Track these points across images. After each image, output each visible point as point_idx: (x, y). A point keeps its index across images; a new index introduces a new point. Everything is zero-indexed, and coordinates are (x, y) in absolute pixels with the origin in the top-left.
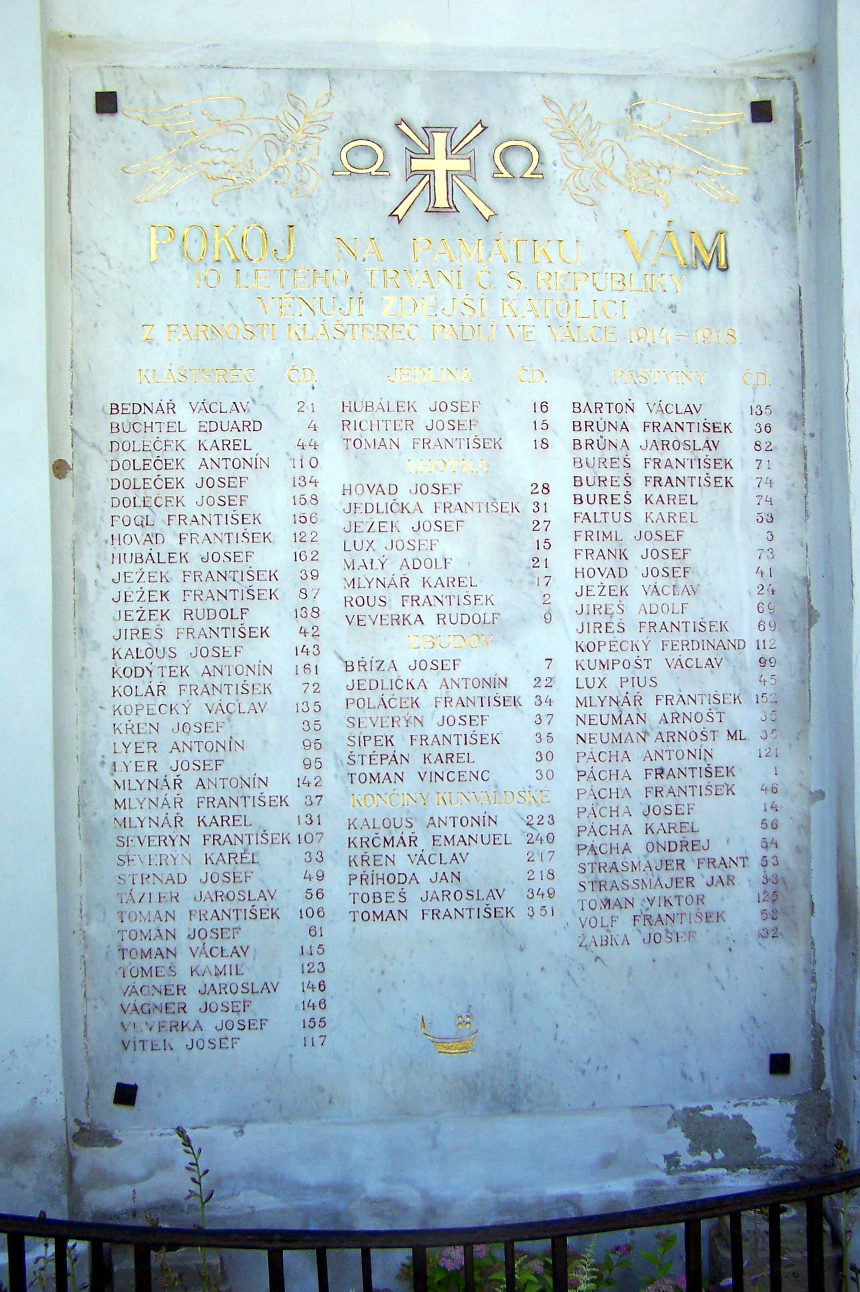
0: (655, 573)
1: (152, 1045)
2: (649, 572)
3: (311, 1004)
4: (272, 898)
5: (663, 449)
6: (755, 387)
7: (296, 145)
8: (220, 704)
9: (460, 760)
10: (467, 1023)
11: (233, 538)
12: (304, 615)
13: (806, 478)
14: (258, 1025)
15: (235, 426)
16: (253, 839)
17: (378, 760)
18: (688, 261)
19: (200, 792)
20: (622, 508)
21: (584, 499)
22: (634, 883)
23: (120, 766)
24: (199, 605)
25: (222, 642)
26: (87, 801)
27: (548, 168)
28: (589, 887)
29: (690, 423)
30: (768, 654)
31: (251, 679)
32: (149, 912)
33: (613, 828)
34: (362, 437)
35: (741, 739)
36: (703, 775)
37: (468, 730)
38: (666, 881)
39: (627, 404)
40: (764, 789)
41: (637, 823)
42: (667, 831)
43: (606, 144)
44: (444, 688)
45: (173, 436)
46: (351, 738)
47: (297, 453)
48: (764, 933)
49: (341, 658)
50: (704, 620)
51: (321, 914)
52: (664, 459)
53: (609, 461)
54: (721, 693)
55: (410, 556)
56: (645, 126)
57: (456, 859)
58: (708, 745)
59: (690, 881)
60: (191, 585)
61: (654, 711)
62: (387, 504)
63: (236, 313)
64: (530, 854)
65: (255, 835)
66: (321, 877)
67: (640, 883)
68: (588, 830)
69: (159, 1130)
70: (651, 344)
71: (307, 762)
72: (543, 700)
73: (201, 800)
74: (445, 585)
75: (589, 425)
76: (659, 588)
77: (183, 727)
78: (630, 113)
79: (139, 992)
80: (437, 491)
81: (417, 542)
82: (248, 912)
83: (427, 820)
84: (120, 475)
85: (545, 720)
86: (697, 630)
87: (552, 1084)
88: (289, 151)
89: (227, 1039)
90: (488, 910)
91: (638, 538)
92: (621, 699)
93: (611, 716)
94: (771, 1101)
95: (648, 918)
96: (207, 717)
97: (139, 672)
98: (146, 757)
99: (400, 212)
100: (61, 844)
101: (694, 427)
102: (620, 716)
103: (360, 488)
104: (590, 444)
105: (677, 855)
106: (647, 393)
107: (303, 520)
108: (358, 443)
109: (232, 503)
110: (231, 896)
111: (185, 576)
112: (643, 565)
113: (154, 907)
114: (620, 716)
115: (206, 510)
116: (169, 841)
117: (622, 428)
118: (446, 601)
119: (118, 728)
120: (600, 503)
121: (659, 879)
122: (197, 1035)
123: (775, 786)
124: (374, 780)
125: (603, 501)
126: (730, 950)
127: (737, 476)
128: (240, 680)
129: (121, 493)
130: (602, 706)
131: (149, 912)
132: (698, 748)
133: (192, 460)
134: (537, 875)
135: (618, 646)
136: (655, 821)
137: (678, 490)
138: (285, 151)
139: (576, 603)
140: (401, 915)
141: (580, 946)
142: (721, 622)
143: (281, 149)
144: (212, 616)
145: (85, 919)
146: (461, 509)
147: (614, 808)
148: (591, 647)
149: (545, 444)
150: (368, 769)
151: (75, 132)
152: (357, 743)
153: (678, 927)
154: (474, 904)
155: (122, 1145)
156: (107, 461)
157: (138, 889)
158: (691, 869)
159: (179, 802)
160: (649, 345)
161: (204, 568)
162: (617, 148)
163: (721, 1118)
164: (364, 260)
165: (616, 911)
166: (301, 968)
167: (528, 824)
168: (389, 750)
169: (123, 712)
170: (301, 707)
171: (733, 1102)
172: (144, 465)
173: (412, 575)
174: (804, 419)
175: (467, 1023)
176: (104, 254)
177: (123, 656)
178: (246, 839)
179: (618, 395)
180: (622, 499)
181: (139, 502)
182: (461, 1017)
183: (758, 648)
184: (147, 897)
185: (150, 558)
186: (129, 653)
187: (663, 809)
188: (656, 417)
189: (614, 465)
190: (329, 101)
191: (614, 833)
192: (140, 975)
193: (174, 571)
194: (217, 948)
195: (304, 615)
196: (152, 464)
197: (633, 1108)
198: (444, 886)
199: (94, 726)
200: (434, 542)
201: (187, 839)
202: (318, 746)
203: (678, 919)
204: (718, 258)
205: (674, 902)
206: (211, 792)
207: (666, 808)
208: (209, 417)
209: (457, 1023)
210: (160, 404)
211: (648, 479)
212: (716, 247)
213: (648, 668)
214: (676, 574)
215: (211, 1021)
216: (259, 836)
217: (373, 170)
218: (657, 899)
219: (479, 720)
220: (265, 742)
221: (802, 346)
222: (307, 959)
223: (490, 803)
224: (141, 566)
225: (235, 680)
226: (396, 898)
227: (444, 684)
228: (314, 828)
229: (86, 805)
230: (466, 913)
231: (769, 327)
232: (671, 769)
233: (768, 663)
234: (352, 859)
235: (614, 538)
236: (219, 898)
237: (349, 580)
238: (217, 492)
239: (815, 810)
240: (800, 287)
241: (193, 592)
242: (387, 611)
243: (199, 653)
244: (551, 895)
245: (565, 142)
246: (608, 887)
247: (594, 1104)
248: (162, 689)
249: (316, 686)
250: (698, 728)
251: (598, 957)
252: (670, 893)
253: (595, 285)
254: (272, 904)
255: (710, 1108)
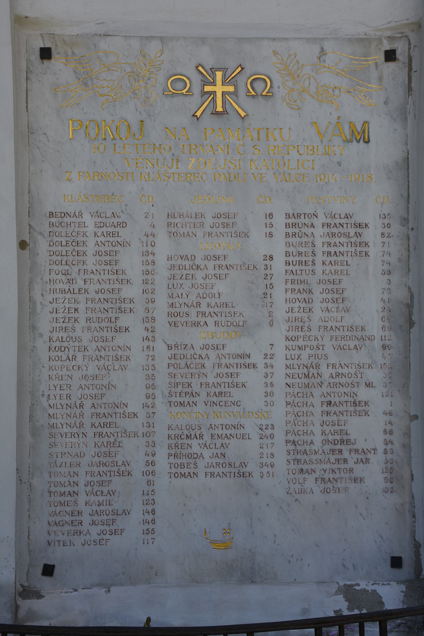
0: (327, 301)
1: (64, 543)
2: (324, 301)
3: (147, 521)
4: (128, 465)
5: (332, 237)
6: (382, 204)
7: (145, 78)
8: (104, 366)
9: (226, 395)
10: (228, 533)
11: (112, 282)
12: (147, 321)
13: (409, 251)
14: (119, 532)
15: (113, 225)
16: (119, 434)
17: (184, 395)
18: (348, 138)
19: (93, 410)
20: (310, 268)
21: (291, 263)
22: (316, 461)
23: (52, 397)
24: (94, 315)
25: (105, 334)
26: (34, 415)
27: (275, 90)
28: (292, 462)
29: (347, 223)
30: (388, 343)
31: (120, 353)
32: (65, 472)
33: (306, 434)
34: (177, 231)
35: (372, 387)
36: (352, 405)
37: (230, 380)
38: (332, 459)
39: (314, 214)
40: (385, 413)
41: (317, 430)
42: (333, 434)
43: (306, 76)
44: (218, 359)
45: (82, 230)
46: (170, 383)
47: (144, 239)
48: (386, 490)
49: (165, 343)
50: (353, 325)
51: (154, 474)
52: (333, 242)
53: (304, 243)
54: (361, 363)
55: (201, 292)
56: (327, 66)
57: (223, 446)
58: (355, 390)
59: (345, 461)
60: (90, 305)
61: (326, 372)
62: (190, 265)
63: (114, 166)
64: (262, 444)
65: (120, 433)
66: (154, 455)
67: (319, 461)
68: (291, 433)
69: (66, 590)
70: (327, 182)
71: (148, 395)
72: (268, 365)
73: (93, 414)
74: (219, 306)
75: (294, 225)
76: (329, 309)
77: (85, 377)
78: (319, 59)
79: (58, 514)
80: (215, 259)
81: (205, 284)
82: (116, 472)
83: (208, 426)
84: (54, 248)
85: (270, 376)
86: (349, 330)
87: (273, 567)
88: (141, 81)
89: (103, 540)
90: (239, 473)
91: (318, 283)
92: (309, 365)
93: (303, 374)
94: (392, 583)
95: (323, 479)
96: (97, 372)
97: (63, 349)
98: (65, 392)
99: (198, 114)
100: (20, 437)
101: (349, 226)
102: (308, 374)
103: (176, 257)
104: (294, 235)
105: (338, 447)
106: (325, 208)
107: (147, 273)
108: (175, 234)
109: (111, 264)
110: (107, 464)
111: (87, 300)
112: (321, 297)
113: (67, 470)
114: (308, 374)
115: (98, 267)
116: (76, 435)
117: (311, 226)
118: (219, 315)
119: (51, 377)
120: (299, 265)
121: (329, 459)
122: (88, 537)
123: (391, 412)
124: (182, 405)
125: (300, 264)
126: (368, 498)
127: (372, 251)
128: (114, 353)
129: (54, 258)
130: (299, 369)
131: (65, 472)
132: (349, 391)
133: (91, 242)
134: (265, 456)
135: (307, 338)
136: (327, 429)
137: (341, 258)
138: (139, 81)
139: (286, 316)
140: (195, 475)
141: (287, 493)
142: (362, 326)
143: (137, 80)
144: (100, 321)
145: (31, 476)
146: (227, 268)
147: (305, 422)
148: (293, 339)
149: (271, 235)
150: (179, 399)
151: (29, 69)
152: (173, 386)
153: (339, 485)
154: (232, 470)
155: (45, 598)
156: (47, 241)
157: (59, 460)
158: (346, 454)
159: (82, 415)
160: (326, 183)
161: (97, 297)
162: (312, 80)
163: (365, 591)
164: (179, 139)
165: (306, 475)
166: (143, 502)
167: (260, 429)
168: (189, 390)
169: (54, 369)
170: (145, 367)
171: (371, 582)
172: (67, 243)
173: (202, 301)
174: (408, 220)
175: (228, 533)
176: (45, 134)
177: (54, 341)
178: (116, 435)
179: (309, 210)
180: (310, 263)
181: (64, 262)
182: (225, 529)
183: (382, 340)
184: (64, 464)
185: (69, 291)
186: (58, 339)
187: (331, 422)
188: (329, 221)
189: (307, 245)
190: (162, 54)
191: (305, 434)
192: (59, 505)
193: (81, 298)
194: (99, 491)
195: (147, 321)
196: (70, 244)
197: (318, 583)
198: (217, 460)
199: (39, 376)
200: (213, 285)
201: (85, 434)
202: (154, 387)
203: (339, 481)
204: (364, 136)
205: (337, 472)
206: (98, 410)
207: (332, 422)
208: (100, 220)
209: (223, 533)
210: (75, 213)
211: (324, 253)
212: (363, 130)
213: (323, 349)
214: (338, 302)
215: (95, 530)
216: (123, 432)
217: (184, 91)
218: (328, 469)
219: (235, 375)
220: (126, 385)
221: (408, 182)
222: (146, 497)
223: (241, 418)
224: (65, 295)
225: (111, 353)
226: (192, 466)
227: (218, 356)
228: (151, 429)
229: (34, 416)
230: (228, 475)
231: (390, 172)
232: (335, 402)
233: (387, 348)
234: (170, 445)
235: (306, 283)
236: (101, 465)
237: (170, 303)
238: (103, 258)
239: (414, 424)
240: (408, 151)
241: (91, 309)
242: (189, 319)
243: (94, 339)
244: (272, 466)
245: (285, 75)
246: (302, 462)
247: (295, 580)
248: (75, 358)
249: (153, 357)
250: (349, 381)
251: (297, 500)
252: (335, 466)
253: (298, 151)
254: (128, 468)
255: (358, 585)
